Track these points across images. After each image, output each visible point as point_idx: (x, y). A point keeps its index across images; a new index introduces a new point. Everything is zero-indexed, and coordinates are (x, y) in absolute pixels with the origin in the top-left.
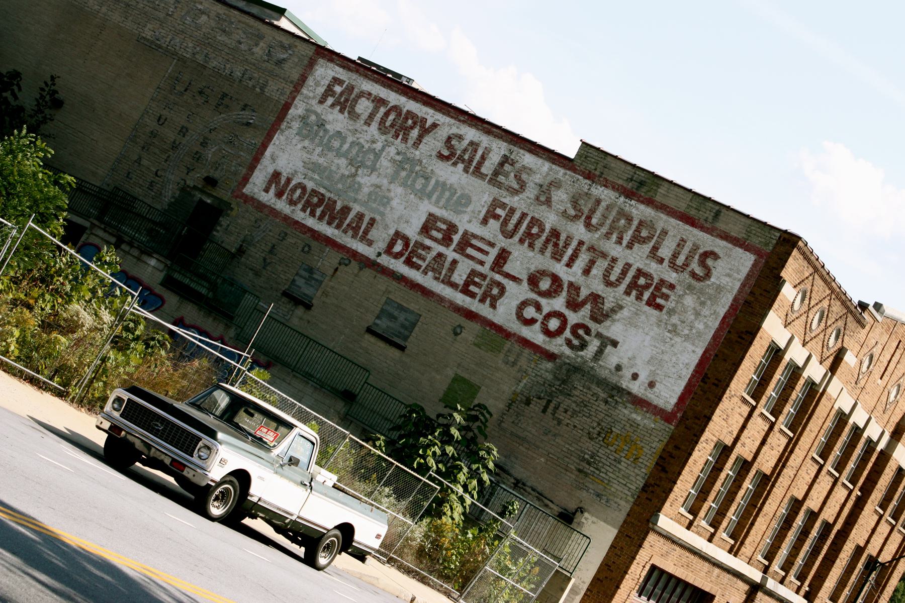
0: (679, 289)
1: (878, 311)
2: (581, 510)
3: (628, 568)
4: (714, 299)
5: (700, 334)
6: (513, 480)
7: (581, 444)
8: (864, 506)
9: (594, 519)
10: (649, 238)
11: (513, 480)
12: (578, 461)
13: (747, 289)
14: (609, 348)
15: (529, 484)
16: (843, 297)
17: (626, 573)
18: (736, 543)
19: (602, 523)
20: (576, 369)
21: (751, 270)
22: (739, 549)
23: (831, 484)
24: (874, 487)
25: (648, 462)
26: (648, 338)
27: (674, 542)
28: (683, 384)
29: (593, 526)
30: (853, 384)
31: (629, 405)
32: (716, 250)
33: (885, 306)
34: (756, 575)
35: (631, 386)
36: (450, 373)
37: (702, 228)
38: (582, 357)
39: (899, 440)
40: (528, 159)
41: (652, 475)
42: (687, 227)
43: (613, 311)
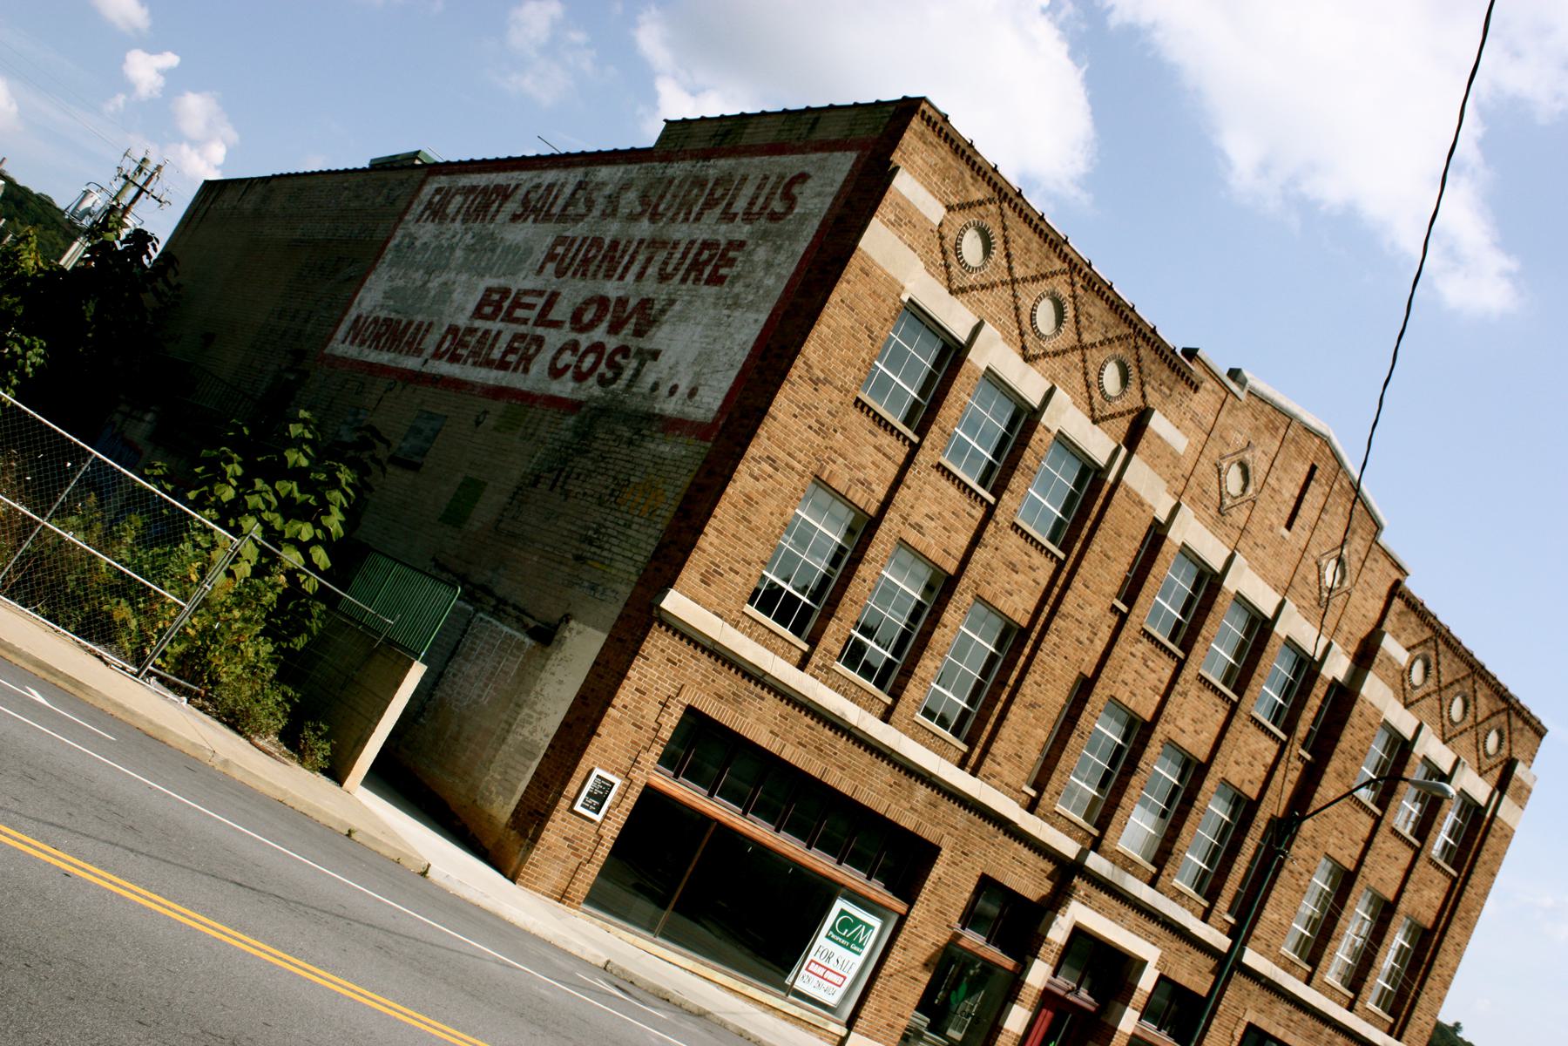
0: (750, 246)
1: (1234, 380)
2: (567, 618)
3: (612, 693)
4: (793, 237)
5: (767, 294)
6: (493, 602)
7: (586, 518)
8: (1320, 778)
9: (581, 626)
10: (723, 196)
11: (493, 602)
12: (577, 544)
13: (842, 201)
14: (649, 364)
15: (511, 601)
16: (1131, 316)
17: (609, 704)
18: (971, 749)
19: (590, 629)
20: (603, 412)
21: (851, 171)
22: (980, 762)
23: (1274, 752)
24: (1334, 746)
25: (667, 512)
26: (699, 328)
27: (690, 641)
28: (734, 374)
29: (577, 639)
30: (1213, 512)
31: (659, 435)
32: (806, 169)
33: (1246, 373)
34: (1069, 848)
35: (665, 406)
36: (459, 479)
37: (793, 150)
38: (613, 392)
39: (1368, 668)
40: (604, 173)
41: (669, 528)
42: (776, 158)
43: (663, 311)
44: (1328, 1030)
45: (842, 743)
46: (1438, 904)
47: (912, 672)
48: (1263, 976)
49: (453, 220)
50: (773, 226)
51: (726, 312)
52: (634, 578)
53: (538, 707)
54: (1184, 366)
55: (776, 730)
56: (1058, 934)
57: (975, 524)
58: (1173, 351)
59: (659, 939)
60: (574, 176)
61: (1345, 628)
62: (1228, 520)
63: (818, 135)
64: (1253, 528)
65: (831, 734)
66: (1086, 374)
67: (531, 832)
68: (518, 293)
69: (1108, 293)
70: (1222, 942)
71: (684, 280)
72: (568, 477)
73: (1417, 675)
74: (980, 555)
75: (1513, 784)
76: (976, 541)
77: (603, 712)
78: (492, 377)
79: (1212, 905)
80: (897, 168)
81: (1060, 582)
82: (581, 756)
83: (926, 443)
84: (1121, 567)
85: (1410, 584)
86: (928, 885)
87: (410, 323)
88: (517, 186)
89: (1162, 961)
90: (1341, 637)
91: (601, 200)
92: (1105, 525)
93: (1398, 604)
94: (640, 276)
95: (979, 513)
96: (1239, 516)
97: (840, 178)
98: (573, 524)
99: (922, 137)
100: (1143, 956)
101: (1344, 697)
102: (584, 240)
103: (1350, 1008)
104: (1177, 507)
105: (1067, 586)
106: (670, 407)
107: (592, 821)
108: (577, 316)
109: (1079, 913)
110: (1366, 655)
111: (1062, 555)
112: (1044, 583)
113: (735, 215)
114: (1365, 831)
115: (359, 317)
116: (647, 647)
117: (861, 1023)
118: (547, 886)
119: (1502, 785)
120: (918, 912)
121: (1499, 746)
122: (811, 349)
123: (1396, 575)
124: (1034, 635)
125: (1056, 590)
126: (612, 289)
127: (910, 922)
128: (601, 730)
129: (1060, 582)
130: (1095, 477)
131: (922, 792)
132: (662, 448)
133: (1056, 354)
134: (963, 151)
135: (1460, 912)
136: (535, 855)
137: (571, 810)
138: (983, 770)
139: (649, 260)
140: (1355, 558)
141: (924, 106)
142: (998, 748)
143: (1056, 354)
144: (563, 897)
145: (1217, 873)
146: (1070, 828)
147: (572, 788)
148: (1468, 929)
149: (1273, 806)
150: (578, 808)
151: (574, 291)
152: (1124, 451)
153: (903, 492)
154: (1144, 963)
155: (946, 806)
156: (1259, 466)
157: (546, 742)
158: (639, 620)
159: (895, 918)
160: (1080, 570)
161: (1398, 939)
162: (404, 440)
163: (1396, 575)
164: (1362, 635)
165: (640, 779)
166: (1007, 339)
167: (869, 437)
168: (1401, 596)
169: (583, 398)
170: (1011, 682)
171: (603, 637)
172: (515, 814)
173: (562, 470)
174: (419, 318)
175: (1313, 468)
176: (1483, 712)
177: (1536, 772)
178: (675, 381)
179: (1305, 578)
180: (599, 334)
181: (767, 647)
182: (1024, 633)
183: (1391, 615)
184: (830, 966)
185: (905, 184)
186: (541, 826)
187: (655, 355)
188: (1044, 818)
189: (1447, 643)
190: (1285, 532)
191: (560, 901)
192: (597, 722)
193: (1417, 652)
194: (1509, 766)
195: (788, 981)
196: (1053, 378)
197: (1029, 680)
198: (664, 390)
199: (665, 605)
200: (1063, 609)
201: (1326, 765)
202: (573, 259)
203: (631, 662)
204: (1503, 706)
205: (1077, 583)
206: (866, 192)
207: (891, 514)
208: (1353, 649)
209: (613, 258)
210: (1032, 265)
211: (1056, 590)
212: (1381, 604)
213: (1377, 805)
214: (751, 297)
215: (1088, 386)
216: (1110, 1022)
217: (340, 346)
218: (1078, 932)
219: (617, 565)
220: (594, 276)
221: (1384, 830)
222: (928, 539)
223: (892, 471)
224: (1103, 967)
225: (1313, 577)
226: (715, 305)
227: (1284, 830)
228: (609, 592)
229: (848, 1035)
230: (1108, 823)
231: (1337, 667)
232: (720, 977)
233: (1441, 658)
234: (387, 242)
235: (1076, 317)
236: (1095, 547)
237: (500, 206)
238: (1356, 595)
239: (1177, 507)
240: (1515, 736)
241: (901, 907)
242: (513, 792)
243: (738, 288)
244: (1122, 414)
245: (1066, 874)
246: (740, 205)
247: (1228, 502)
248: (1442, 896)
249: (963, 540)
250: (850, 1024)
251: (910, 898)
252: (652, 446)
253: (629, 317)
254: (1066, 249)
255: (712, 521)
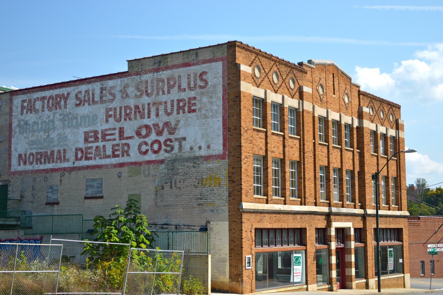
0: (198, 98)
1: (311, 64)
2: (208, 222)
5: (217, 111)
8: (364, 155)
9: (216, 223)
10: (175, 83)
11: (174, 227)
12: (196, 201)
13: (226, 78)
14: (183, 142)
15: (181, 224)
17: (242, 239)
18: (302, 199)
22: (305, 201)
24: (364, 144)
25: (225, 182)
26: (197, 127)
30: (320, 102)
31: (204, 162)
32: (204, 70)
33: (313, 60)
34: (326, 209)
35: (201, 153)
38: (174, 153)
39: (363, 119)
40: (110, 83)
43: (177, 125)
44: (388, 218)
45: (282, 216)
46: (396, 169)
47: (285, 189)
48: (372, 214)
49: (43, 111)
50: (202, 90)
51: (204, 120)
52: (227, 204)
53: (217, 248)
54: (300, 67)
55: (270, 222)
56: (333, 233)
57: (282, 142)
58: (295, 65)
59: (269, 288)
60: (97, 86)
61: (354, 111)
62: (323, 102)
63: (201, 58)
64: (328, 100)
65: (279, 215)
66: (287, 87)
67: (240, 280)
68: (102, 131)
69: (289, 64)
70: (361, 211)
71: (178, 113)
72: (175, 183)
73: (371, 113)
74: (287, 149)
75: (400, 126)
76: (284, 147)
77: (242, 242)
78: (114, 161)
79: (355, 203)
80: (240, 64)
81: (302, 145)
82: (242, 255)
83: (268, 130)
84: (311, 132)
85: (362, 89)
86: (308, 239)
87: (52, 152)
88: (68, 94)
89: (353, 225)
90: (354, 115)
91: (117, 93)
92: (305, 124)
93: (361, 96)
94: (157, 115)
95: (282, 139)
96: (325, 99)
97: (221, 71)
98: (189, 196)
99: (239, 52)
100: (349, 226)
101: (360, 129)
102: (121, 108)
103: (389, 210)
104: (314, 106)
105: (304, 145)
106: (203, 153)
107: (249, 269)
108: (138, 134)
109: (335, 224)
110: (360, 116)
111: (299, 137)
112: (298, 147)
113: (185, 89)
114: (376, 161)
115: (20, 156)
116: (243, 220)
117: (309, 282)
118: (248, 291)
119: (397, 128)
120: (308, 247)
121: (393, 118)
122: (243, 124)
123: (357, 89)
124: (302, 162)
125: (302, 147)
126: (146, 121)
127: (308, 250)
128: (243, 246)
129: (302, 145)
130: (296, 112)
131: (298, 216)
132: (208, 165)
133: (280, 87)
134: (258, 53)
135: (401, 168)
136: (244, 285)
137: (246, 269)
138: (307, 203)
139: (157, 109)
140: (349, 91)
141: (237, 43)
142: (307, 195)
143: (280, 87)
144: (252, 291)
145: (352, 194)
146: (323, 205)
147: (244, 264)
148: (404, 172)
149: (357, 169)
150: (247, 268)
151: (130, 127)
152: (301, 101)
153: (269, 145)
154: (350, 228)
155: (304, 216)
156: (323, 82)
157: (228, 256)
158: (236, 215)
159: (304, 252)
160: (305, 139)
161: (392, 184)
162: (86, 190)
163: (357, 89)
164: (357, 110)
165: (253, 252)
166: (272, 91)
167: (258, 136)
168: (361, 94)
169: (163, 158)
170: (302, 177)
171: (227, 223)
172: (230, 277)
173: (171, 182)
174: (56, 149)
175: (333, 74)
176: (387, 111)
177: (404, 119)
178: (199, 145)
179: (342, 105)
180: (154, 136)
181: (260, 203)
182: (299, 163)
183: (361, 101)
184: (297, 271)
185: (244, 68)
186: (242, 277)
187: (184, 139)
188: (319, 206)
189: (374, 99)
190: (334, 96)
191: (252, 292)
192: (242, 244)
193: (369, 106)
194: (397, 122)
195: (292, 280)
196: (282, 93)
197: (306, 173)
198: (196, 148)
199: (244, 208)
200: (305, 151)
201: (364, 150)
202: (120, 115)
203: (242, 225)
204: (390, 106)
205: (306, 142)
206: (233, 76)
207: (269, 153)
208: (357, 116)
209: (139, 112)
210: (268, 67)
211: (302, 147)
212: (358, 99)
213: (385, 155)
214: (211, 114)
215: (288, 90)
216: (349, 247)
217: (15, 166)
218: (337, 229)
219: (216, 202)
220: (135, 118)
221: (379, 158)
222: (276, 153)
223: (264, 141)
224: (342, 233)
225: (343, 103)
226: (198, 119)
227: (362, 173)
228: (219, 210)
229: (308, 286)
230: (330, 197)
231: (356, 124)
232: (282, 290)
233: (374, 104)
234: (11, 124)
235: (280, 74)
236: (305, 131)
237: (65, 102)
238: (352, 101)
239: (314, 106)
240: (395, 113)
241: (304, 247)
242: (225, 273)
243: (203, 112)
244: (296, 92)
245: (328, 216)
246: (184, 85)
247: (322, 97)
248: (396, 166)
249: (281, 148)
250: (307, 283)
251: (306, 245)
252: (204, 166)
253: (163, 129)
254: (273, 58)
255: (243, 180)
